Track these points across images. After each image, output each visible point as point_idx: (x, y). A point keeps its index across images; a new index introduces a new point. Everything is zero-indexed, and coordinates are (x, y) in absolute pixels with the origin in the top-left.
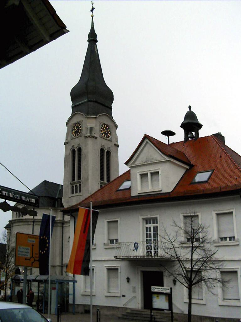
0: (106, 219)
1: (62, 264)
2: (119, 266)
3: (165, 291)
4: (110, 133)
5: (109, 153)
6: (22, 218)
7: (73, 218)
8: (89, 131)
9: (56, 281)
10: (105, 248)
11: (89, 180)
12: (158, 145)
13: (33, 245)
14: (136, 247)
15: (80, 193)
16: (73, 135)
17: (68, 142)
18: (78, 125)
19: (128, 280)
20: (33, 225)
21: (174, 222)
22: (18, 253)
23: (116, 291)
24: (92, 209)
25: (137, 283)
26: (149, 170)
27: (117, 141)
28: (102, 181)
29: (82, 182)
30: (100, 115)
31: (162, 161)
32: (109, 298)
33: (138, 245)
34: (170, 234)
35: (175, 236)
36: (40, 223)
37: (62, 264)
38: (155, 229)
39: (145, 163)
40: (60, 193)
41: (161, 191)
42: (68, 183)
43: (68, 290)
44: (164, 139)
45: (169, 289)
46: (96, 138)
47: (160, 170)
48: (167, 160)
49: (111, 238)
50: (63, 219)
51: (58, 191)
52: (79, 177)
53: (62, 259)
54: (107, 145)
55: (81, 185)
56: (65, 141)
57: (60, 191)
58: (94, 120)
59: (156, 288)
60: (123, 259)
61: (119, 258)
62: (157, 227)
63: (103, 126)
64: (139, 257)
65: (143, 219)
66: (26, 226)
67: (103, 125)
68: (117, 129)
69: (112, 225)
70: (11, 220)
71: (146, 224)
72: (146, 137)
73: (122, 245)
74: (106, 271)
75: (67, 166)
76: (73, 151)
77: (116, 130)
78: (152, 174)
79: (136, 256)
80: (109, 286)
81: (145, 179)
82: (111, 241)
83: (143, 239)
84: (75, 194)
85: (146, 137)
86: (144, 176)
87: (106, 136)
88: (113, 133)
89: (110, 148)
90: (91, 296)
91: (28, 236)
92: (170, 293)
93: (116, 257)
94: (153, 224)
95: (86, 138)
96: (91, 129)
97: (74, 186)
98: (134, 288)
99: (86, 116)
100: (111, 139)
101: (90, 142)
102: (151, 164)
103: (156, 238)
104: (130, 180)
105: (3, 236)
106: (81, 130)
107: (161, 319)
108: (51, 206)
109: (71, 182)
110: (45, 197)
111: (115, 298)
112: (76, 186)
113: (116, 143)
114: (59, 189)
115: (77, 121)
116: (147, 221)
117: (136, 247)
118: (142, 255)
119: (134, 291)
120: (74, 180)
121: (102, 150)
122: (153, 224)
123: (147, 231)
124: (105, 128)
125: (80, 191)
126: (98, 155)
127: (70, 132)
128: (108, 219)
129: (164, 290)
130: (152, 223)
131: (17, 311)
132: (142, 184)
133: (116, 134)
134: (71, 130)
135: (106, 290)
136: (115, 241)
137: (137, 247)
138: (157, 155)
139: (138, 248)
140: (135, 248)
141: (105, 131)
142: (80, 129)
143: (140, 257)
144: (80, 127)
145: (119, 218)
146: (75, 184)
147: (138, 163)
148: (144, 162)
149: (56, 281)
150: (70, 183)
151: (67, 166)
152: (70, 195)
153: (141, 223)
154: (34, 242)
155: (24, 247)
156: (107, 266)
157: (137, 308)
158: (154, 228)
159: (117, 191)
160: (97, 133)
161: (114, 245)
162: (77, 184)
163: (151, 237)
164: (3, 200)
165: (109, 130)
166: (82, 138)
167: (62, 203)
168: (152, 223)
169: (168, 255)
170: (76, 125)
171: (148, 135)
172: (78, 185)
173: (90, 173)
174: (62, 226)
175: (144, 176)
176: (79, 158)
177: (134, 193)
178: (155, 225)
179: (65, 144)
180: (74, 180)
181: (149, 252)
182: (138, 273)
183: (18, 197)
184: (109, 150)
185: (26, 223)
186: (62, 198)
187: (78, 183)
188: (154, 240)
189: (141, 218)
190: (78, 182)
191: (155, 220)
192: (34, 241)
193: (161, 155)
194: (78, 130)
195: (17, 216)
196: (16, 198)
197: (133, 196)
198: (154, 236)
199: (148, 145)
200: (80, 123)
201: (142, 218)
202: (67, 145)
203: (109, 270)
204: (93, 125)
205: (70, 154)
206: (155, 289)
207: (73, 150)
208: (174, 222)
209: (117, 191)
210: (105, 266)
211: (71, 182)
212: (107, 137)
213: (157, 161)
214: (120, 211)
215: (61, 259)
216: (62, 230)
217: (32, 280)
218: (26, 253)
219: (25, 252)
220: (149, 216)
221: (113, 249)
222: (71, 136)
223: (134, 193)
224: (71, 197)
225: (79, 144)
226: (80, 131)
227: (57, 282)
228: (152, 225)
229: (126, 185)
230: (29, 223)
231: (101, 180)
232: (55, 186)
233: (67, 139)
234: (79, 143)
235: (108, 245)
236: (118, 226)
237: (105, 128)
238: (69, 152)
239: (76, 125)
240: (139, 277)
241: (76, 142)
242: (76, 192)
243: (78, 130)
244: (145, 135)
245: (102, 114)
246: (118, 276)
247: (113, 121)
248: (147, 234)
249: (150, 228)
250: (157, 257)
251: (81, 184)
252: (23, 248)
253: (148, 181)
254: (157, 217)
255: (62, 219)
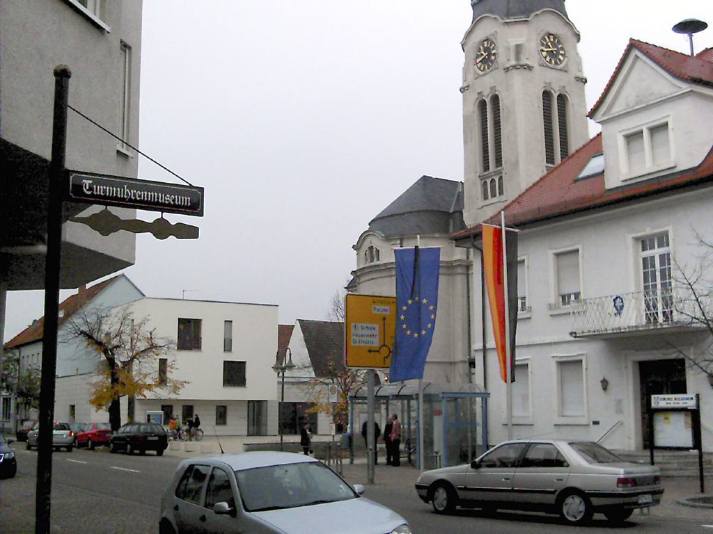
0: (550, 249)
2: (583, 354)
3: (684, 403)
4: (562, 52)
5: (562, 99)
6: (378, 263)
7: (479, 252)
8: (512, 56)
9: (441, 395)
10: (551, 315)
11: (521, 166)
12: (664, 61)
13: (384, 319)
14: (619, 308)
15: (502, 196)
16: (479, 68)
17: (468, 86)
18: (487, 44)
19: (605, 384)
21: (698, 236)
22: (352, 338)
23: (577, 413)
24: (506, 226)
25: (626, 389)
26: (643, 121)
27: (580, 71)
28: (550, 165)
29: (504, 172)
30: (537, 15)
31: (673, 95)
32: (563, 429)
33: (622, 302)
34: (686, 266)
35: (697, 270)
36: (394, 272)
38: (665, 258)
39: (633, 107)
40: (458, 200)
41: (675, 167)
42: (475, 177)
43: (474, 415)
44: (680, 44)
45: (692, 399)
46: (530, 68)
47: (671, 117)
48: (686, 91)
49: (565, 292)
50: (468, 258)
51: (454, 196)
52: (499, 161)
54: (557, 82)
55: (504, 178)
56: (461, 86)
57: (458, 196)
58: (522, 29)
59: (661, 399)
60: (593, 337)
61: (580, 335)
62: (668, 254)
63: (545, 40)
64: (625, 329)
65: (636, 239)
66: (388, 278)
67: (546, 37)
68: (579, 41)
69: (566, 261)
70: (355, 270)
71: (643, 250)
72: (634, 45)
73: (588, 304)
74: (553, 367)
76: (482, 104)
77: (579, 44)
78: (654, 130)
79: (620, 329)
80: (562, 402)
81: (635, 145)
82: (565, 299)
83: (637, 285)
84: (491, 200)
85: (634, 45)
86: (633, 138)
87: (553, 62)
88: (570, 54)
89: (564, 87)
90: (510, 426)
91: (372, 299)
92: (695, 408)
93: (574, 335)
94: (659, 247)
95: (507, 71)
96: (518, 48)
98: (619, 402)
99: (504, 21)
100: (567, 65)
101: (517, 78)
102: (647, 108)
103: (667, 281)
104: (602, 154)
105: (333, 307)
106: (494, 54)
107: (681, 469)
108: (438, 232)
109: (481, 175)
110: (427, 211)
111: (577, 428)
112: (493, 181)
113: (579, 74)
114: (457, 192)
115: (485, 35)
116: (645, 243)
117: (619, 308)
118: (633, 323)
119: (619, 410)
120: (486, 168)
121: (547, 95)
122: (659, 247)
123: (645, 267)
124: (549, 44)
125: (501, 193)
126: (539, 107)
127: (472, 62)
128: (556, 249)
129: (681, 402)
130: (656, 246)
131: (292, 470)
132: (629, 159)
133: (577, 54)
134: (473, 56)
135: (505, 411)
136: (573, 297)
137: (622, 307)
138: (664, 84)
139: (624, 308)
140: (617, 310)
141: (550, 50)
143: (627, 330)
144: (493, 48)
145: (579, 243)
146: (489, 177)
147: (616, 110)
148: (631, 105)
149: (441, 395)
150: (480, 176)
152: (481, 203)
153: (631, 250)
154: (388, 313)
155: (365, 325)
156: (556, 357)
157: (627, 449)
159: (576, 181)
160: (532, 55)
161: (572, 306)
162: (494, 178)
163: (654, 279)
164: (101, 206)
165: (560, 46)
166: (500, 74)
167: (463, 221)
168: (656, 246)
169: (684, 316)
170: (483, 46)
171: (639, 41)
173: (522, 149)
174: (466, 272)
175: (633, 138)
176: (495, 118)
177: (613, 181)
178: (663, 250)
179: (463, 90)
180: (486, 168)
181: (650, 318)
182: (626, 367)
183: (140, 196)
184: (548, 89)
186: (464, 210)
187: (495, 175)
189: (629, 237)
190: (496, 173)
191: (663, 239)
192: (385, 310)
193: (671, 82)
194: (489, 55)
195: (366, 260)
196: (136, 198)
197: (611, 189)
198: (663, 277)
199: (639, 64)
200: (493, 38)
201: (633, 238)
202: (467, 92)
203: (563, 364)
204: (520, 41)
205: (474, 112)
206: (658, 401)
207: (480, 101)
208: (698, 236)
209: (576, 181)
210: (553, 357)
211: (481, 173)
212: (556, 63)
213: (661, 97)
214: (583, 226)
215: (467, 347)
216: (465, 281)
217: (391, 397)
218: (368, 339)
219: (367, 336)
220: (648, 231)
221: (567, 317)
222: (475, 73)
223: (612, 182)
224: (483, 207)
225: (493, 88)
226: (493, 58)
227: (443, 398)
228: (656, 252)
229: (594, 165)
231: (547, 162)
232: (451, 187)
233: (465, 81)
234: (492, 85)
235: (559, 308)
236: (578, 262)
237: (550, 41)
238: (474, 109)
239: (483, 46)
240: (631, 375)
241: (486, 84)
242: (494, 195)
243: (489, 55)
244: (631, 40)
245: (541, 11)
246: (582, 377)
247: (569, 24)
248: (645, 274)
249: (653, 258)
250: (667, 326)
251: (503, 175)
252: (363, 329)
253: (643, 150)
254: (668, 231)
255: (464, 257)
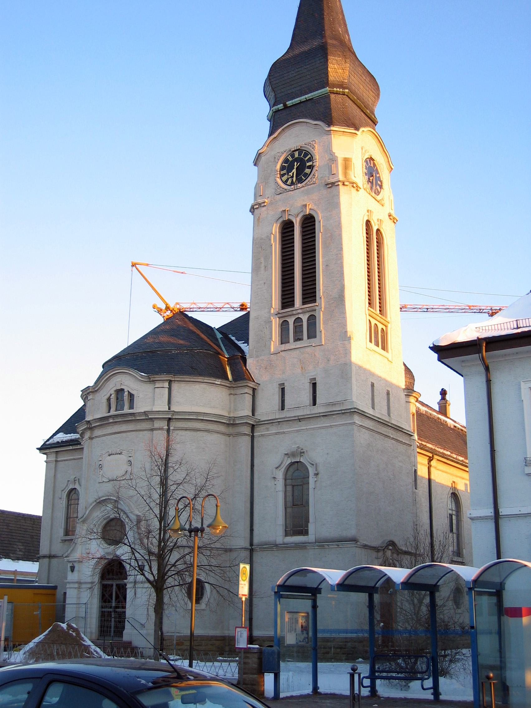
1: (251, 544)
20: (168, 431)
37: (251, 544)
53: (252, 530)
75: (263, 268)
84: (292, 345)
97: (291, 321)
142: (308, 164)
151: (263, 268)
158: (117, 585)
172: (305, 318)
185: (146, 425)
188: (116, 627)
230: (157, 424)
242: (298, 339)
